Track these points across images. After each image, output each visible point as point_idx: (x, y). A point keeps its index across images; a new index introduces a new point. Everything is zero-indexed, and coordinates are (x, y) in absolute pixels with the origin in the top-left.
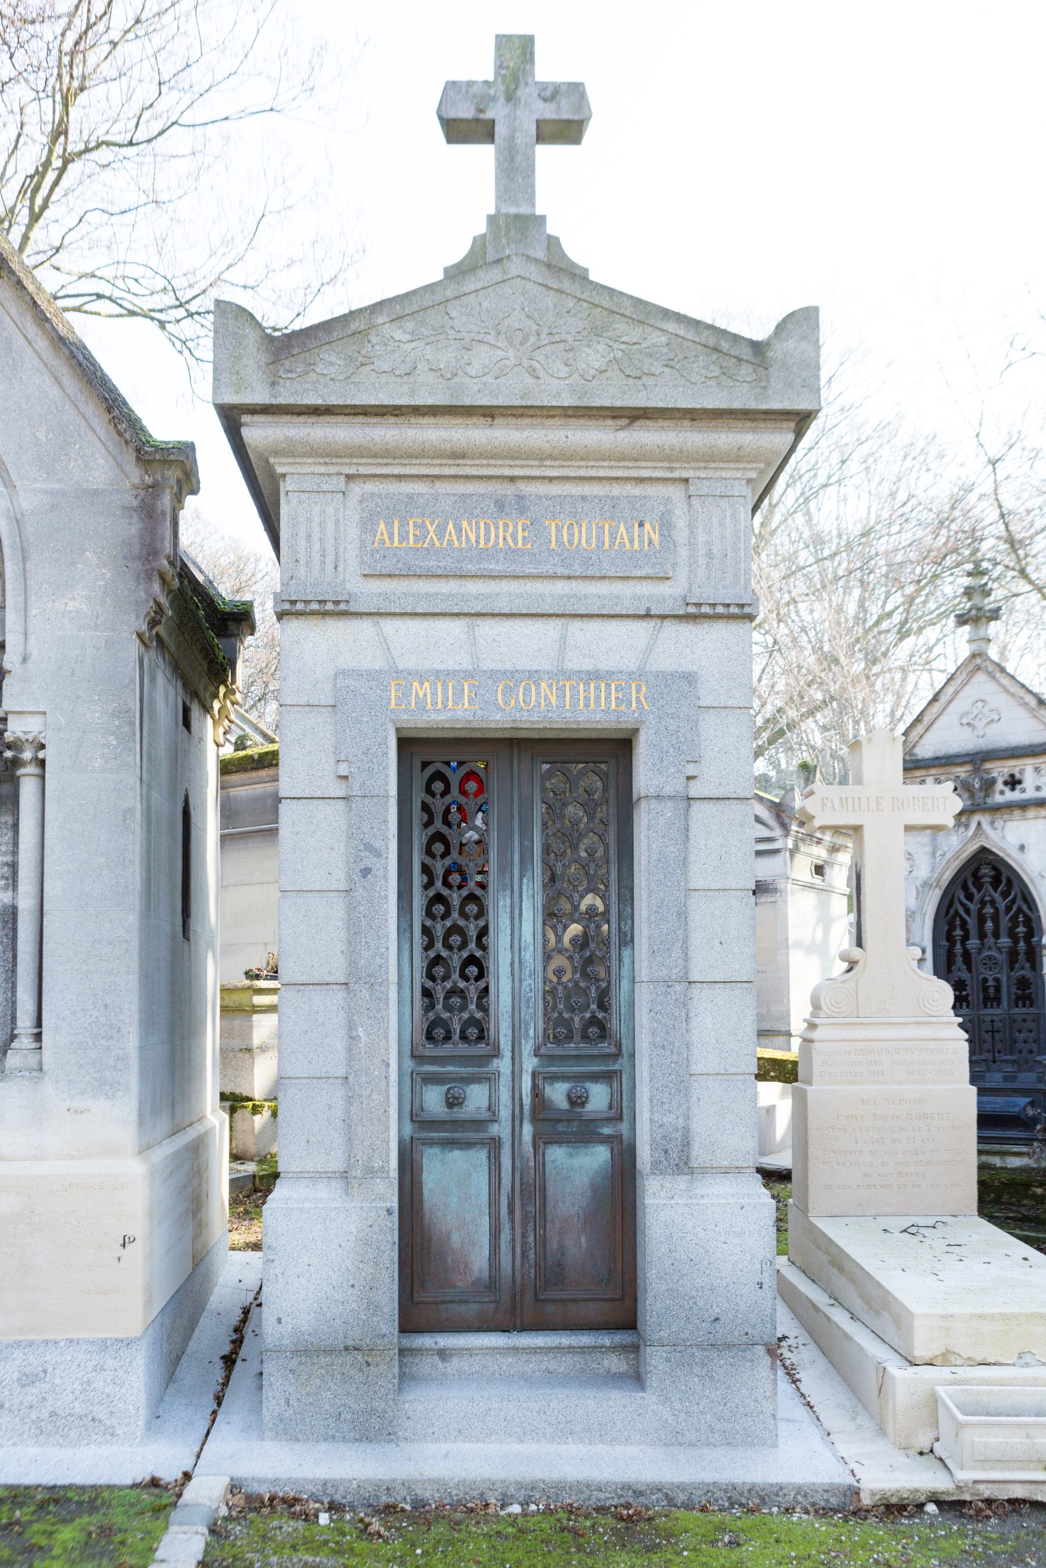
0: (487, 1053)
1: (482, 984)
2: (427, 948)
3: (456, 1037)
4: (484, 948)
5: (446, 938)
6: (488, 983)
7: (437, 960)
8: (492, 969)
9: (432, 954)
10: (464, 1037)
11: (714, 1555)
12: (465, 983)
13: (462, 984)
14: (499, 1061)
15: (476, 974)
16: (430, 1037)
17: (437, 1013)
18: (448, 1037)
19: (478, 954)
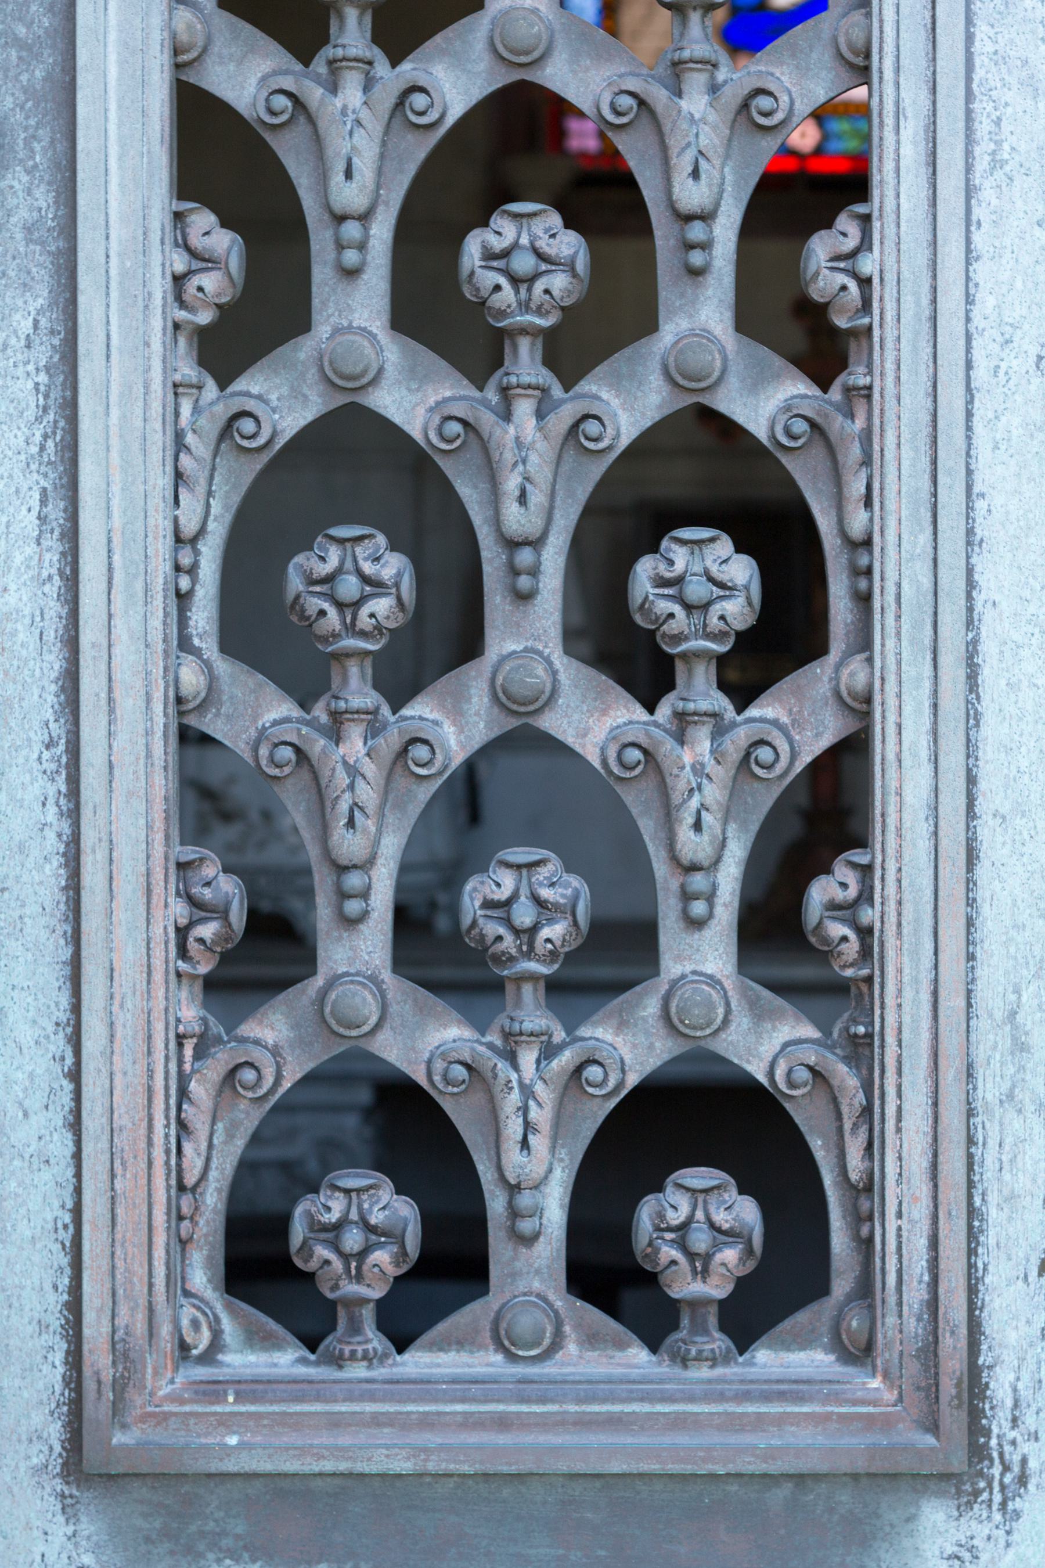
0: (853, 1447)
1: (797, 720)
2: (231, 342)
3: (532, 1265)
4: (822, 345)
5: (430, 229)
6: (860, 707)
7: (349, 464)
8: (903, 566)
9: (283, 399)
10: (610, 1277)
11: (992, 146)
12: (626, 712)
13: (593, 720)
14: (979, 1526)
15: (737, 612)
16: (261, 1266)
17: (323, 1020)
18: (451, 1264)
19: (765, 401)
